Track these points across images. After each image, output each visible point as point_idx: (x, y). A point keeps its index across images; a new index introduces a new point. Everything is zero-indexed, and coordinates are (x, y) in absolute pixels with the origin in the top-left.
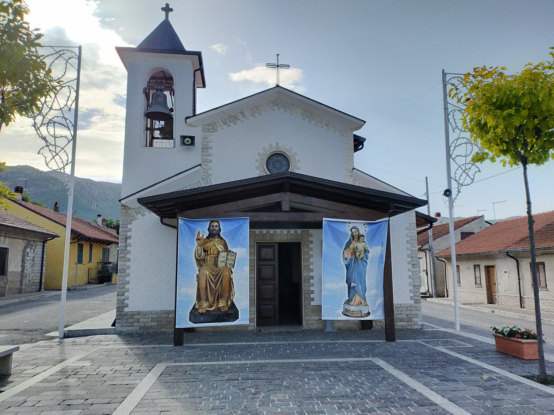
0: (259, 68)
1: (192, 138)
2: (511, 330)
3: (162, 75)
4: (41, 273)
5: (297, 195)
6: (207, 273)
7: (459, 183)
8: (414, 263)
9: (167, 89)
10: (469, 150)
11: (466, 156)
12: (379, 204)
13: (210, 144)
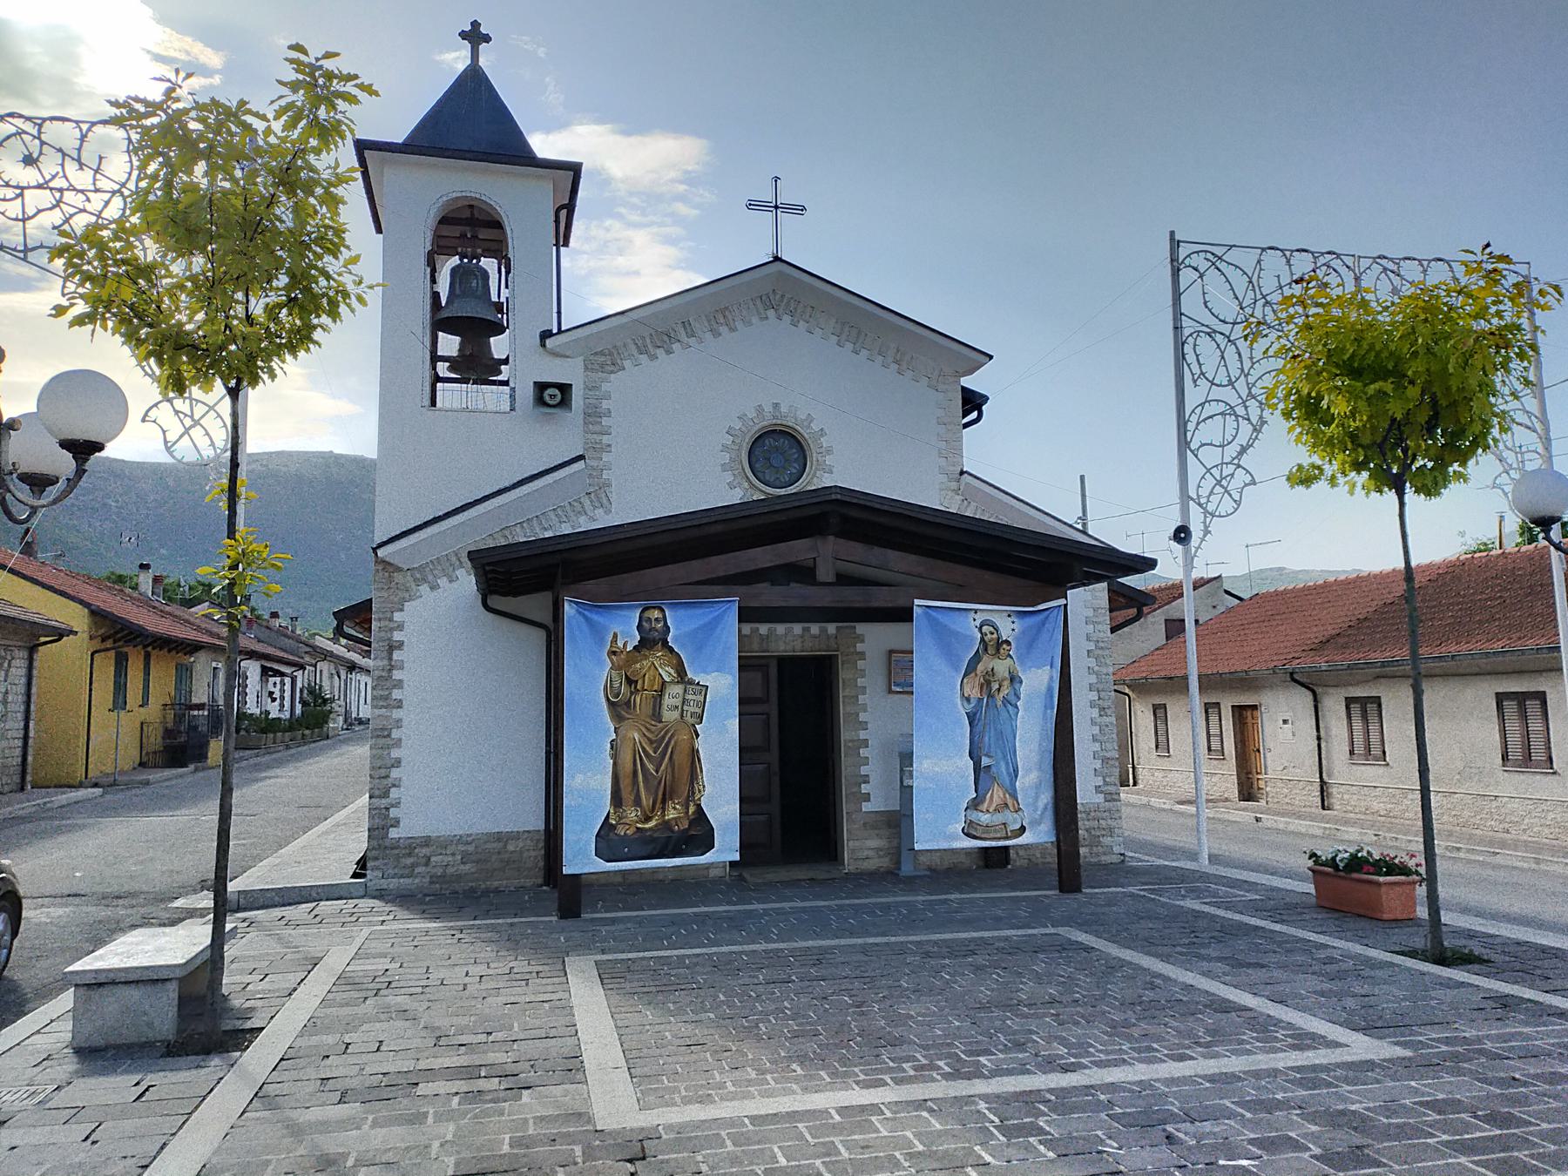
0: (581, 129)
1: (565, 389)
2: (1354, 857)
3: (467, 214)
4: (26, 738)
5: (852, 543)
6: (637, 736)
7: (1206, 512)
8: (1106, 704)
9: (489, 253)
10: (1230, 432)
11: (1222, 446)
12: (1032, 563)
13: (605, 404)
